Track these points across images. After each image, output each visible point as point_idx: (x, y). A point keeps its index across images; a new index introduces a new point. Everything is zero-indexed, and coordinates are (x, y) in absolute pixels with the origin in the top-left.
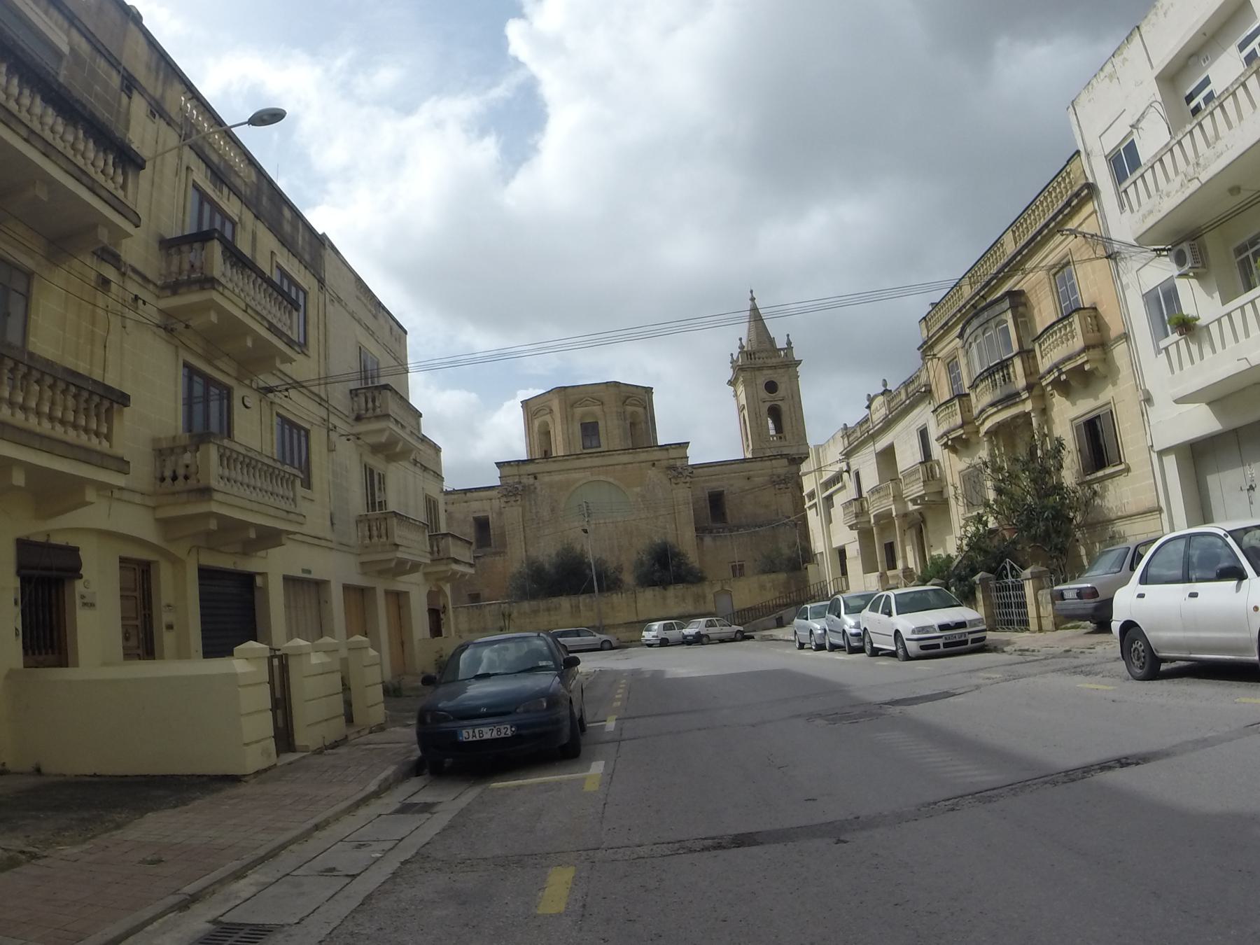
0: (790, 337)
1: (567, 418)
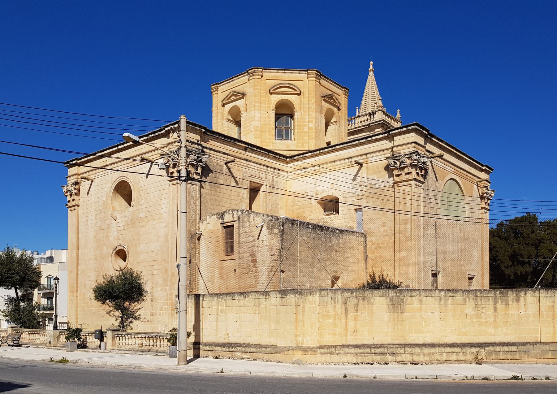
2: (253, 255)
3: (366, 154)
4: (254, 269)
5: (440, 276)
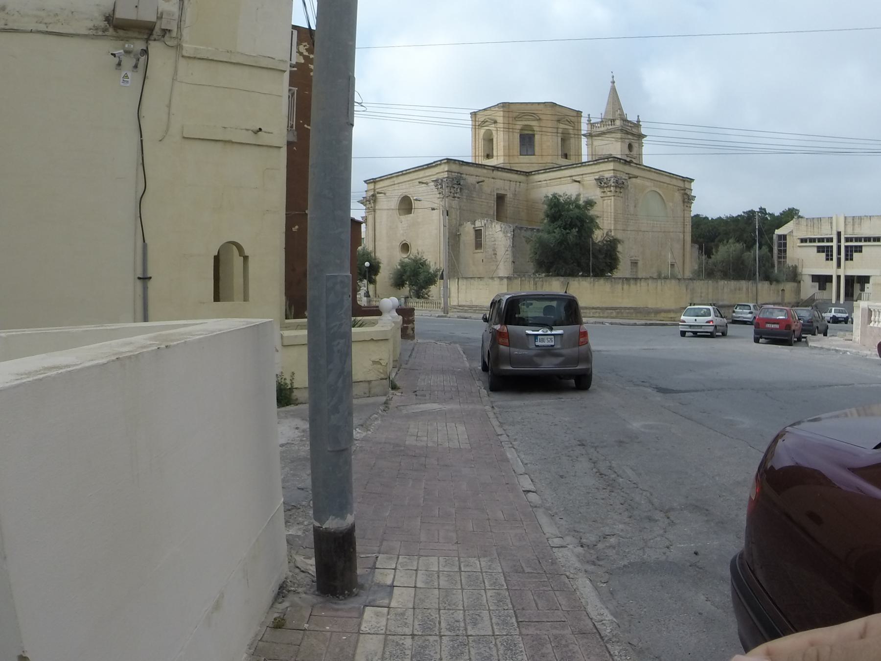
0: (640, 118)
1: (508, 129)
2: (494, 250)
3: (582, 175)
4: (495, 260)
5: (640, 264)
